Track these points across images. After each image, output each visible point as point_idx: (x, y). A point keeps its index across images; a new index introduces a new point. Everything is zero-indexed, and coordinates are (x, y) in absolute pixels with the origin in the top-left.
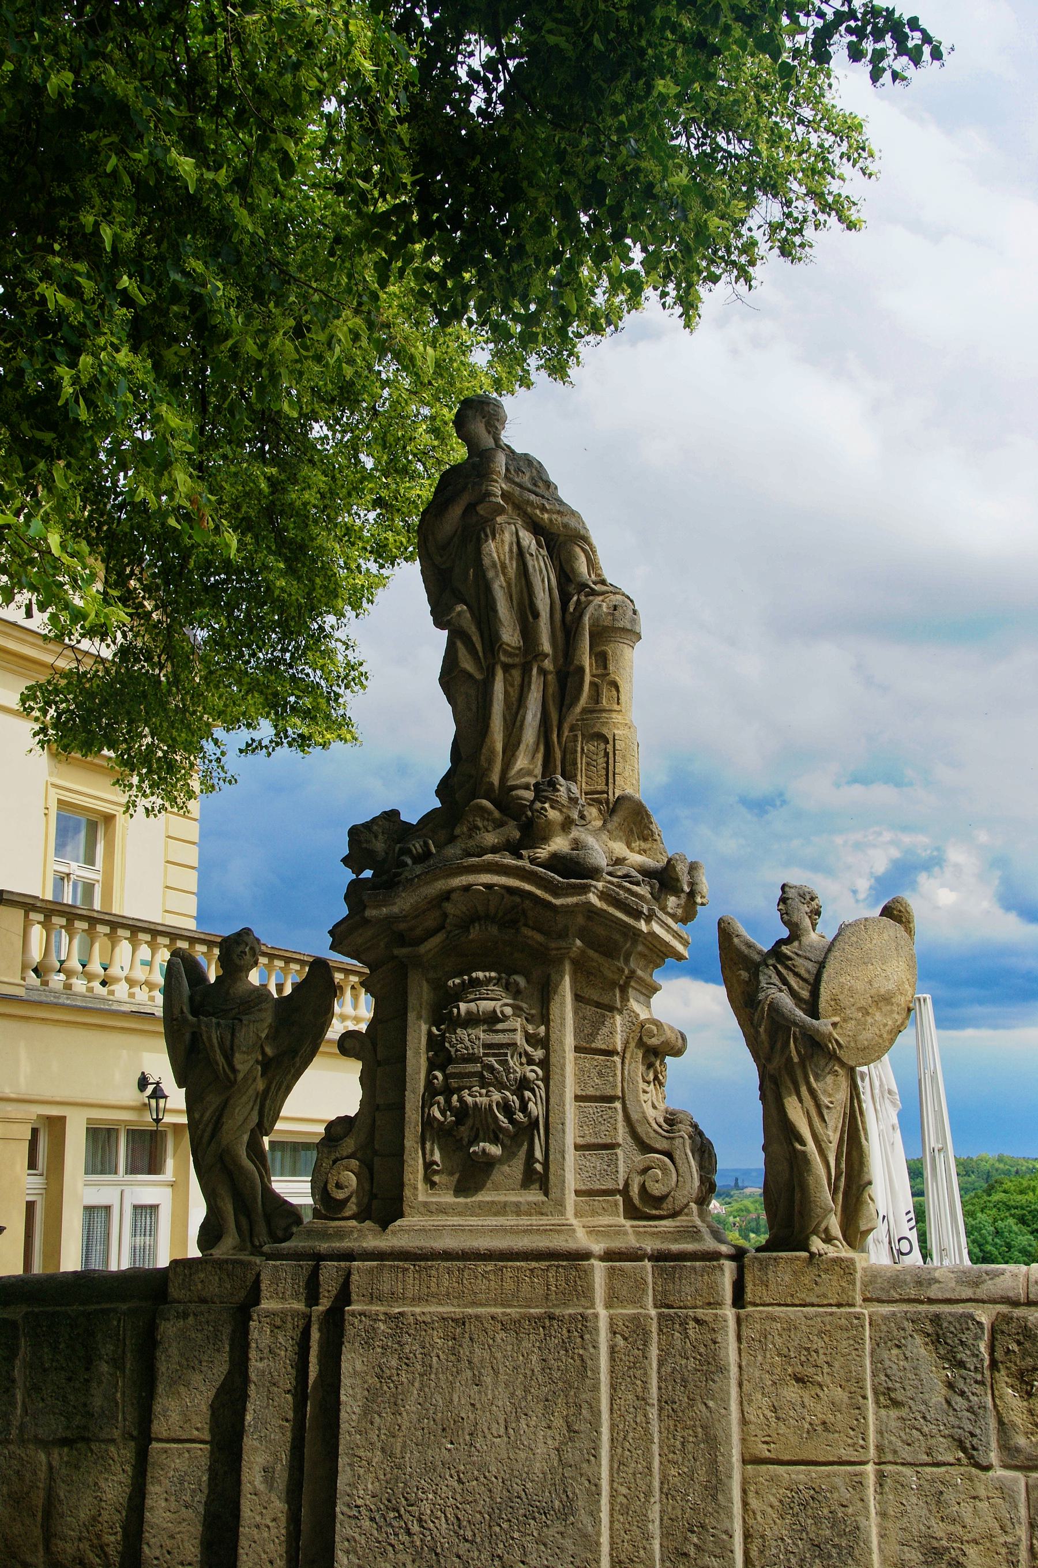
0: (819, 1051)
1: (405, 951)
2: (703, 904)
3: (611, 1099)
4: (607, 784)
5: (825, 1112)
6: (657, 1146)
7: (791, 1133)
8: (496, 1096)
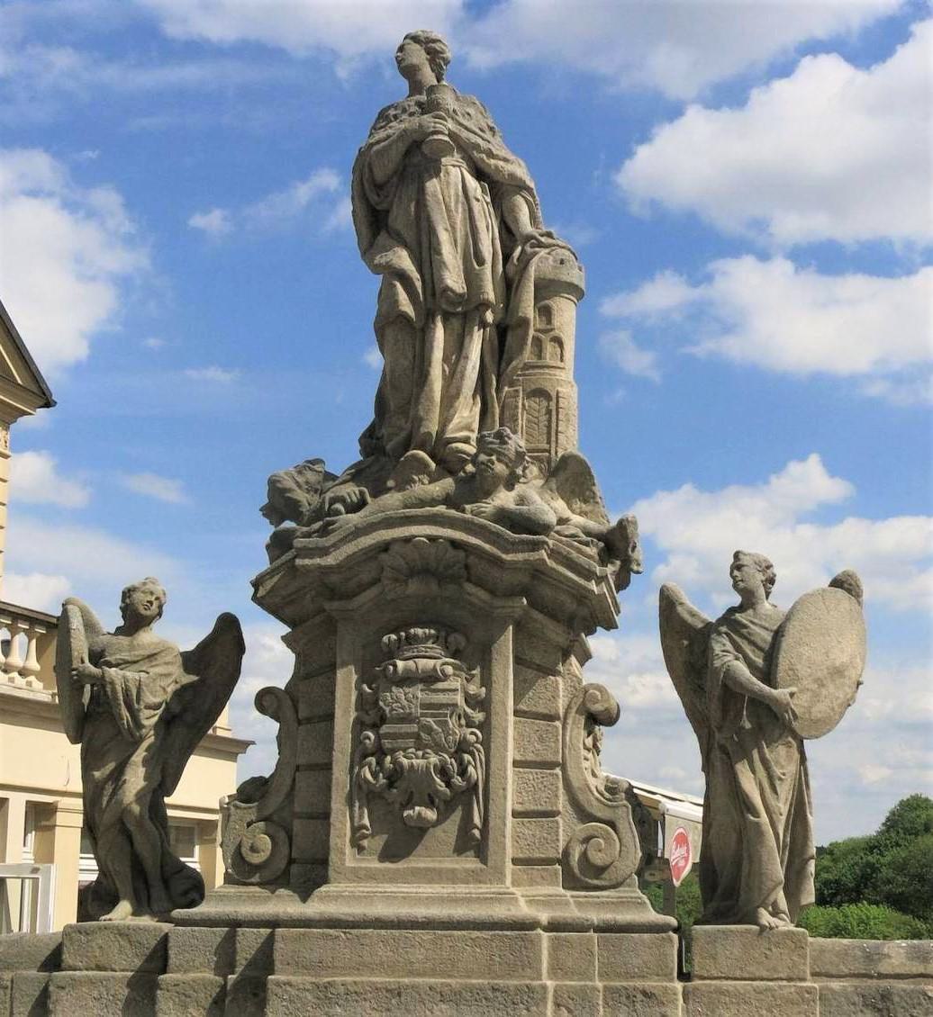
0: (772, 722)
1: (336, 605)
2: (638, 572)
3: (552, 765)
4: (549, 442)
5: (777, 783)
6: (599, 814)
7: (745, 805)
8: (434, 759)
